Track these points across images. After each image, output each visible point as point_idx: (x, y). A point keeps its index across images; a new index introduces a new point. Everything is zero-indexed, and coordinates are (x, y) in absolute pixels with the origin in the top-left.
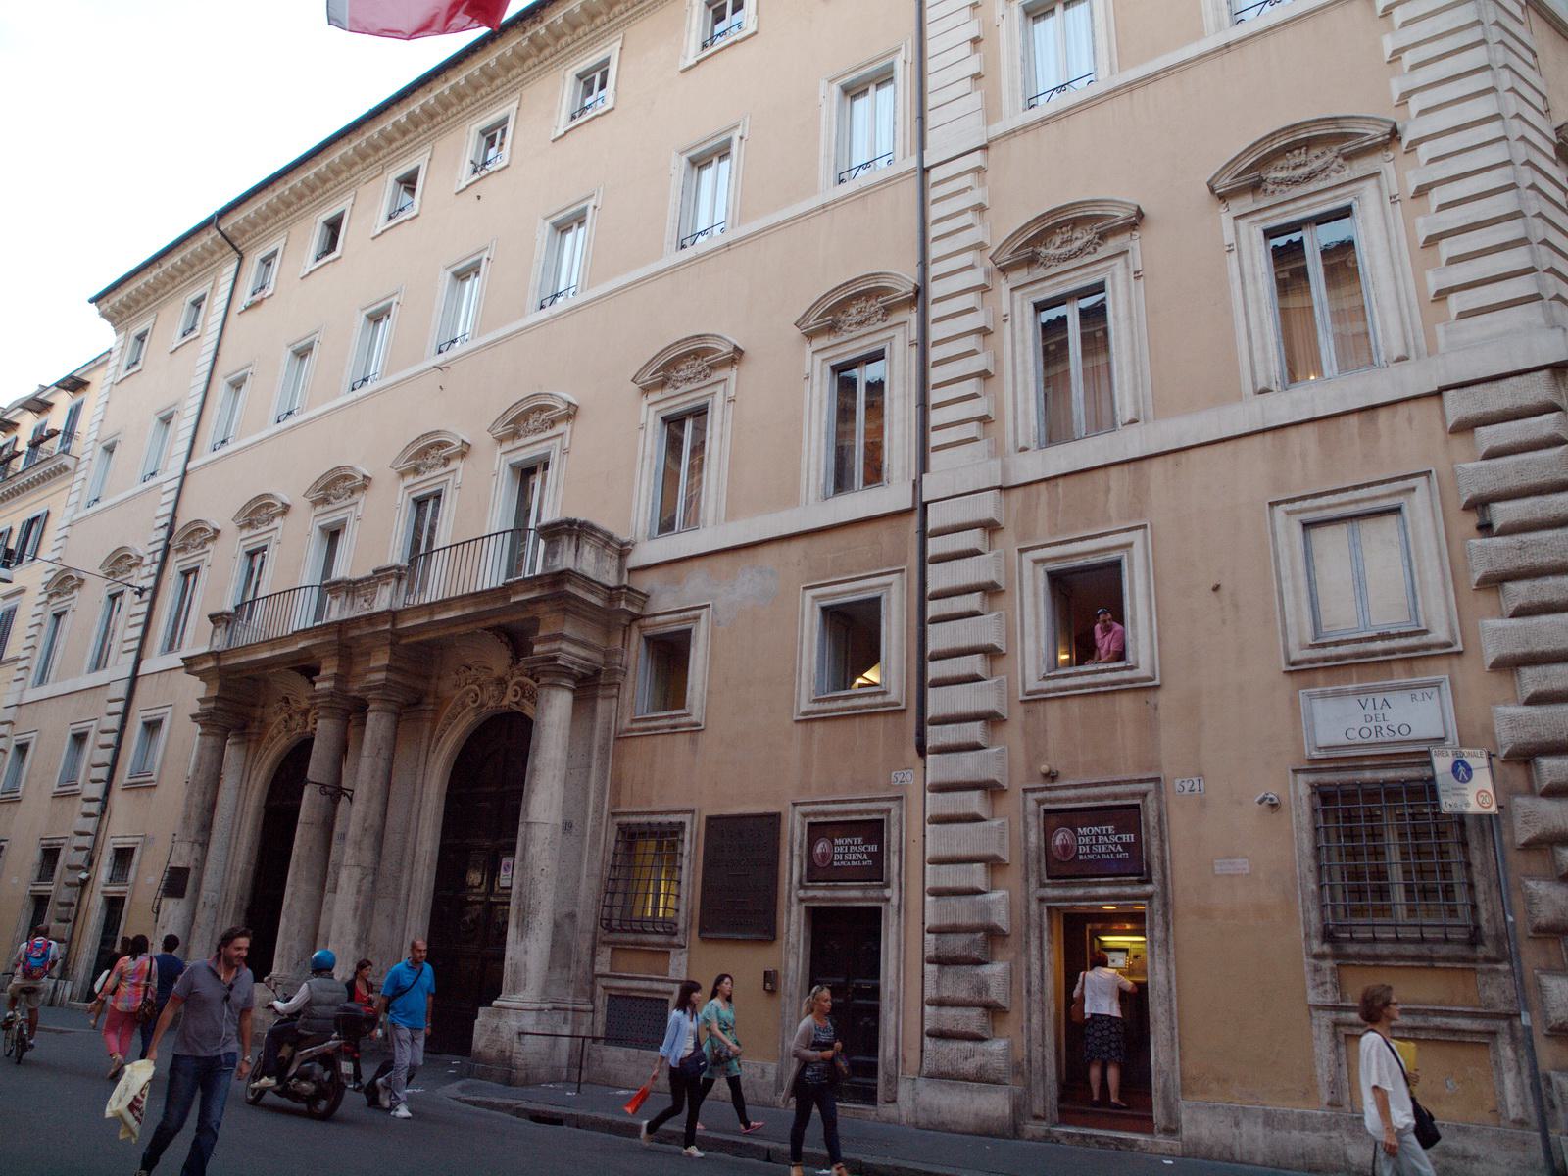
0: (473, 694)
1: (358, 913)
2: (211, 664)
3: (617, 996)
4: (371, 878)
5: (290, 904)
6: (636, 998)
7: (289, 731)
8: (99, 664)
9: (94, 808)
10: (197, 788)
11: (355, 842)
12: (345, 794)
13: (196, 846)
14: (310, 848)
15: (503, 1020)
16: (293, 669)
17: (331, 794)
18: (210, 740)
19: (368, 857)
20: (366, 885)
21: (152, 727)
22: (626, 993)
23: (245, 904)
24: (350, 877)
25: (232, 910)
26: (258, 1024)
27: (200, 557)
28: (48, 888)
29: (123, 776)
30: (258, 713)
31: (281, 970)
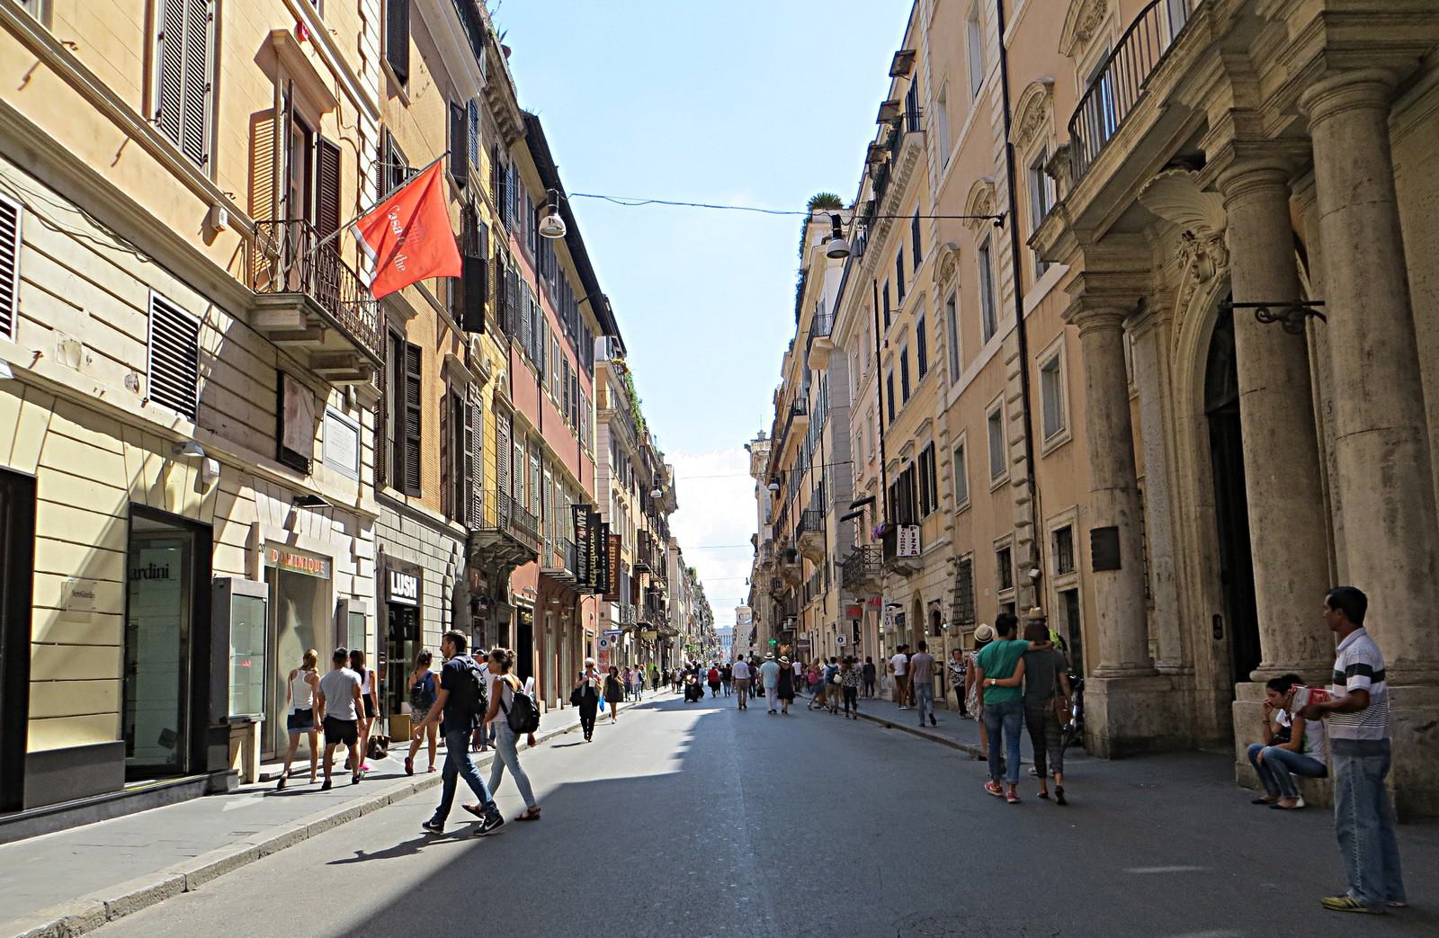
1: (1400, 523)
4: (1409, 448)
5: (1261, 540)
7: (1205, 280)
8: (991, 331)
9: (1024, 491)
10: (1096, 410)
11: (1352, 385)
12: (1313, 313)
13: (1118, 493)
14: (1272, 433)
16: (1169, 166)
17: (1281, 318)
18: (1095, 337)
19: (1390, 406)
20: (1402, 461)
21: (1051, 369)
23: (1217, 567)
24: (1360, 454)
25: (1198, 580)
27: (1044, 133)
28: (1011, 595)
29: (1041, 445)
30: (1156, 281)
31: (1276, 657)
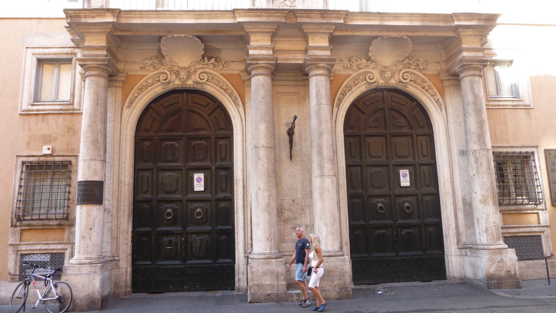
0: (166, 77)
2: (110, 19)
3: (508, 237)
6: (521, 236)
10: (99, 118)
15: (505, 255)
22: (515, 235)
26: (268, 288)
